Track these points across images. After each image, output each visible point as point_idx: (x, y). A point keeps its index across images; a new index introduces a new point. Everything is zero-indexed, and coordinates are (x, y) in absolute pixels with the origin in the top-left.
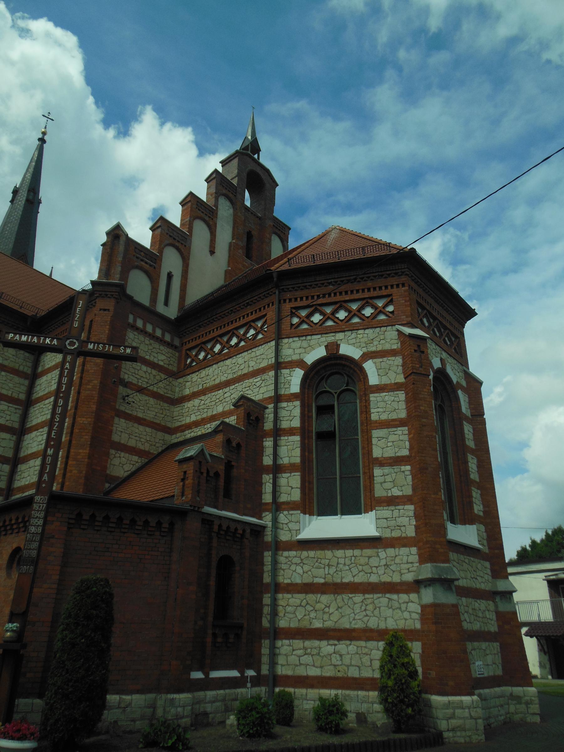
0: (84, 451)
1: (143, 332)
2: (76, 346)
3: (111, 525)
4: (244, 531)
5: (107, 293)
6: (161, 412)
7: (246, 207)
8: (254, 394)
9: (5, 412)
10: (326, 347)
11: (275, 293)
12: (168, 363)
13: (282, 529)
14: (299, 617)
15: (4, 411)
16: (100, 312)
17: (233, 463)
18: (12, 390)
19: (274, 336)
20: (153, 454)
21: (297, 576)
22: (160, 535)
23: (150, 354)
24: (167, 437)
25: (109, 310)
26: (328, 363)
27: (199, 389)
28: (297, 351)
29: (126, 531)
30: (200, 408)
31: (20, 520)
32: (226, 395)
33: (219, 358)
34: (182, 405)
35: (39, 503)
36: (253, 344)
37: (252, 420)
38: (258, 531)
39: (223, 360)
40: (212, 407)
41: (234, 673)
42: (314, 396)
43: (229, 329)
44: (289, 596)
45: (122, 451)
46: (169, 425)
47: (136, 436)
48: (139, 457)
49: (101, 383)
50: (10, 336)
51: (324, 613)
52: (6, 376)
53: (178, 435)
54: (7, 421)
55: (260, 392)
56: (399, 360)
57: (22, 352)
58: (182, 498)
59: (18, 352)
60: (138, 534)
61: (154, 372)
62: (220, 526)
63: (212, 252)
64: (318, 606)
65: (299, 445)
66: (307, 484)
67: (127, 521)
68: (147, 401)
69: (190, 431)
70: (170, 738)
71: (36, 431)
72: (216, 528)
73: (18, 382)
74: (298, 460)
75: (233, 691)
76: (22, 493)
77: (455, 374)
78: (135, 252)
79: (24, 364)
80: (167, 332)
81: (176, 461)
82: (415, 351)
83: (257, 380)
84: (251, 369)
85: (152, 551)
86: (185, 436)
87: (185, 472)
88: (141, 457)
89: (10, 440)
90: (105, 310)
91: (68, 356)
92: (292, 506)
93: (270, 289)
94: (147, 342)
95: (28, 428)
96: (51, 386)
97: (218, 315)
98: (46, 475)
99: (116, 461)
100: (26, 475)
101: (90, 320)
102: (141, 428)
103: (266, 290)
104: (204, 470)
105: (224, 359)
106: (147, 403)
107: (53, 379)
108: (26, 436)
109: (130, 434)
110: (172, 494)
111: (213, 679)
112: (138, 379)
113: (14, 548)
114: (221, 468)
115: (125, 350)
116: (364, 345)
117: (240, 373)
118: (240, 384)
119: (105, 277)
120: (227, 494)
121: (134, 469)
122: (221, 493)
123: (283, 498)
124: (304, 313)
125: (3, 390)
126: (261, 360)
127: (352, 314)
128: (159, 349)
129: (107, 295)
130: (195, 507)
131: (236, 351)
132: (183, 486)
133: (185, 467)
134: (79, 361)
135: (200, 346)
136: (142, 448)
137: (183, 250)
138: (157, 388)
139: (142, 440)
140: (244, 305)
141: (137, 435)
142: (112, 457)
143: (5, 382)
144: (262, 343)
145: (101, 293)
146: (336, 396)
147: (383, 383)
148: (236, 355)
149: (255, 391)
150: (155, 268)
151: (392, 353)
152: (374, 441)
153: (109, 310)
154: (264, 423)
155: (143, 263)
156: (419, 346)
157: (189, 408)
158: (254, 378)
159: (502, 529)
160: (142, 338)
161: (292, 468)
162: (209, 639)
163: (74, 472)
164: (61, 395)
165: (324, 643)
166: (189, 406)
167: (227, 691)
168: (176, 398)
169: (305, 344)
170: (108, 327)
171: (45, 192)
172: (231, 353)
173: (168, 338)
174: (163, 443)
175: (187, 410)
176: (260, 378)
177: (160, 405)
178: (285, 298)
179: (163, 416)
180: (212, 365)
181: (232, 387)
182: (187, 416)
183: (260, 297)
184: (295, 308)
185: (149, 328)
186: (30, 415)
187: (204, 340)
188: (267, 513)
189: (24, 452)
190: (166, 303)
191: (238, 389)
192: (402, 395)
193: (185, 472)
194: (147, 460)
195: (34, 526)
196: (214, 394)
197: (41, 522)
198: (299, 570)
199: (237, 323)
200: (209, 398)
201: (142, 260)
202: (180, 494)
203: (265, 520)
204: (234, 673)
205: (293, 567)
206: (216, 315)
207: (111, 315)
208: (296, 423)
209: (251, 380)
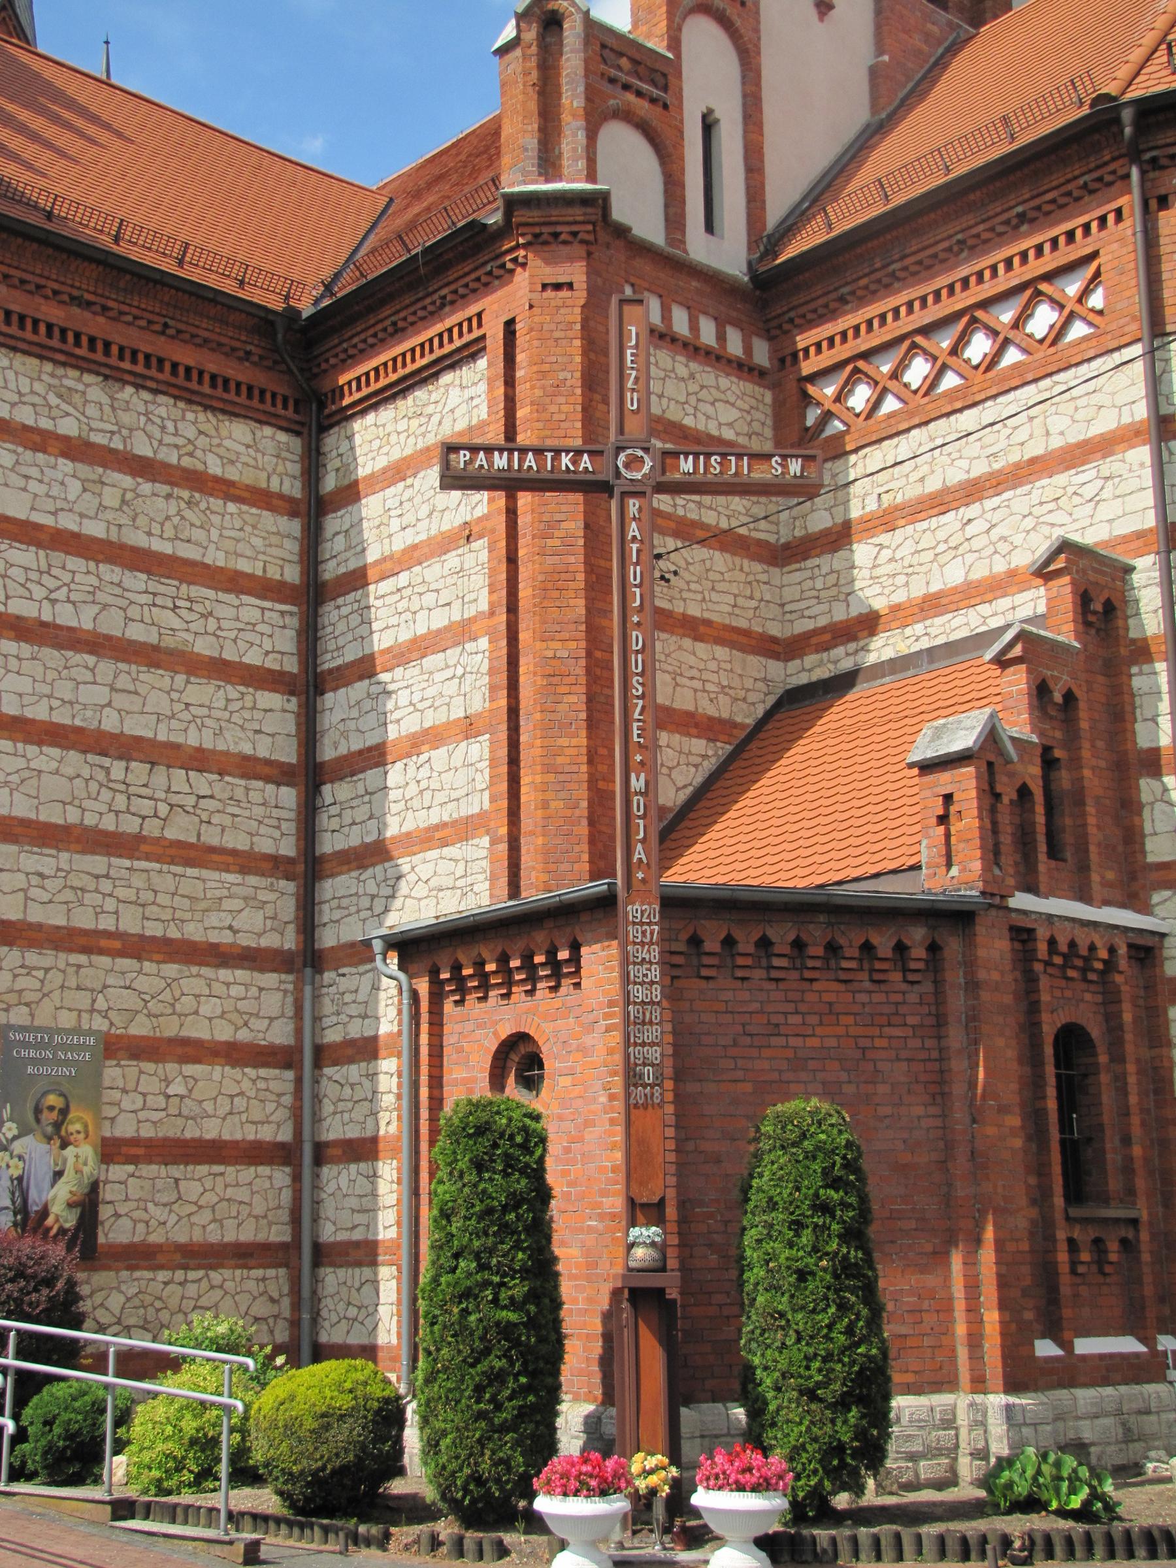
0: (574, 741)
2: (646, 469)
3: (776, 962)
4: (1112, 950)
5: (559, 229)
6: (748, 593)
8: (1077, 526)
9: (258, 628)
11: (1127, 176)
12: (746, 429)
15: (254, 625)
16: (545, 294)
17: (1058, 753)
18: (261, 557)
19: (1134, 327)
20: (743, 726)
22: (905, 981)
23: (695, 408)
24: (775, 668)
25: (570, 286)
27: (868, 509)
29: (815, 975)
30: (878, 572)
32: (970, 530)
34: (809, 563)
35: (642, 923)
37: (1095, 613)
39: (948, 415)
40: (923, 569)
41: (1129, 1345)
43: (959, 306)
46: (774, 630)
47: (692, 678)
48: (709, 740)
49: (587, 526)
50: (462, 460)
52: (241, 513)
53: (810, 660)
54: (267, 653)
55: (1096, 520)
57: (268, 431)
58: (948, 870)
59: (259, 434)
60: (845, 982)
62: (1052, 942)
67: (816, 950)
68: (708, 563)
70: (1073, 1491)
71: (367, 682)
72: (1042, 948)
73: (274, 529)
75: (1136, 1389)
76: (358, 868)
78: (605, 61)
79: (280, 469)
80: (730, 323)
81: (911, 766)
85: (889, 1025)
86: (836, 662)
88: (714, 740)
89: (285, 711)
90: (558, 287)
91: (631, 501)
93: (1106, 164)
94: (682, 371)
95: (331, 671)
96: (390, 536)
97: (907, 262)
98: (639, 847)
100: (361, 814)
101: (505, 318)
102: (701, 648)
103: (1092, 165)
104: (1009, 794)
105: (949, 409)
106: (708, 570)
107: (393, 513)
108: (329, 696)
109: (674, 673)
110: (912, 861)
111: (1084, 1358)
113: (503, 1036)
115: (784, 466)
117: (1015, 457)
118: (1019, 491)
119: (540, 174)
121: (699, 780)
122: (1042, 847)
125: (240, 560)
126: (1092, 411)
128: (718, 388)
129: (556, 235)
130: (993, 895)
132: (948, 835)
133: (945, 781)
135: (849, 368)
136: (712, 711)
137: (738, 23)
138: (729, 517)
139: (710, 687)
140: (1007, 222)
141: (695, 673)
143: (241, 534)
144: (1091, 354)
145: (537, 230)
148: (995, 397)
149: (1079, 513)
153: (570, 286)
154: (1126, 618)
155: (630, 97)
157: (838, 572)
158: (1073, 472)
162: (1063, 1257)
163: (553, 805)
164: (635, 619)
166: (836, 566)
167: (1123, 1389)
168: (782, 541)
170: (577, 343)
172: (975, 389)
173: (735, 345)
174: (765, 689)
175: (832, 579)
176: (1093, 473)
177: (741, 570)
178: (1163, 191)
179: (754, 604)
180: (908, 430)
181: (989, 503)
182: (835, 599)
183: (1069, 194)
186: (329, 629)
187: (865, 343)
188: (1167, 893)
189: (336, 746)
190: (710, 227)
191: (1014, 510)
193: (948, 798)
194: (729, 748)
195: (642, 984)
196: (925, 525)
199: (986, 286)
200: (909, 542)
201: (626, 87)
202: (943, 860)
203: (1162, 915)
204: (1129, 1345)
206: (902, 259)
207: (582, 302)
209: (1061, 479)
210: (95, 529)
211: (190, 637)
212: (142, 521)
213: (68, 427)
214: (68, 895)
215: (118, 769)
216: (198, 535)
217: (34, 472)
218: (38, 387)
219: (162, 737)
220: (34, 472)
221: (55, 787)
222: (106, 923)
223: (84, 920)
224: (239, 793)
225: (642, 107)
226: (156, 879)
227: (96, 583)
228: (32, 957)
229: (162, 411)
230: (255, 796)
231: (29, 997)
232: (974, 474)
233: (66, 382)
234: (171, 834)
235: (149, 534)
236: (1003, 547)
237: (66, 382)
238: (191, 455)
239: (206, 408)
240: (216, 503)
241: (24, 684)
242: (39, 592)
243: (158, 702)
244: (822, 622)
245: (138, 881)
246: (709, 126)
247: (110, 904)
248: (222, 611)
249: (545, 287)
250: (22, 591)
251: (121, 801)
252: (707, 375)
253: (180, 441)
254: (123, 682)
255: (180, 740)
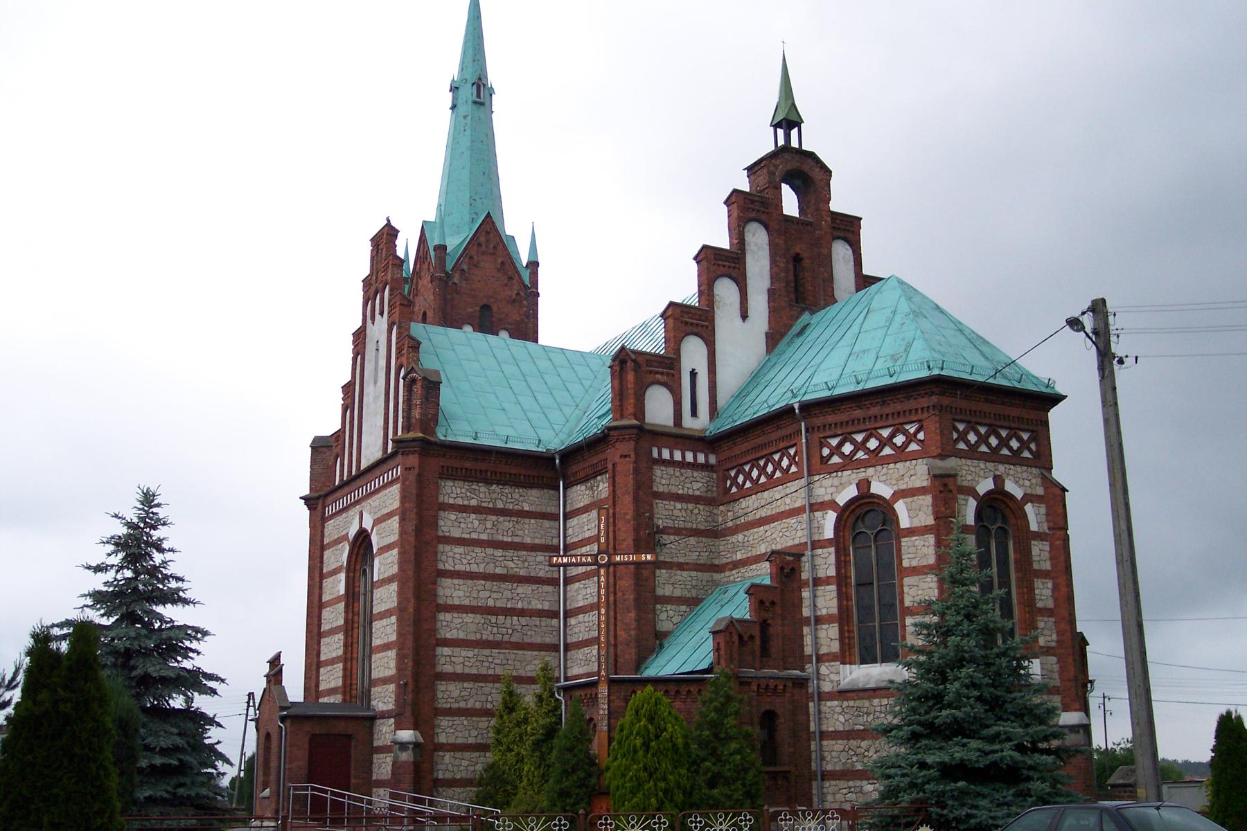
1: (671, 463)
7: (789, 219)
10: (857, 485)
12: (704, 489)
13: (824, 680)
14: (844, 761)
21: (840, 724)
25: (629, 456)
26: (862, 501)
28: (830, 490)
31: (588, 697)
33: (758, 489)
36: (787, 478)
38: (801, 683)
42: (851, 538)
44: (834, 742)
45: (667, 604)
46: (716, 562)
51: (865, 756)
56: (928, 499)
57: (546, 491)
61: (690, 506)
63: (744, 316)
64: (859, 751)
65: (835, 595)
66: (846, 635)
69: (737, 570)
74: (834, 611)
77: (1020, 486)
82: (941, 492)
83: (792, 521)
84: (787, 508)
87: (718, 643)
92: (832, 657)
99: (663, 616)
100: (577, 630)
102: (685, 574)
104: (735, 638)
112: (673, 520)
114: (756, 632)
116: (894, 482)
120: (765, 651)
123: (823, 650)
124: (834, 442)
127: (883, 443)
129: (624, 438)
131: (772, 483)
132: (719, 655)
134: (611, 569)
136: (688, 595)
139: (688, 587)
142: (658, 612)
146: (872, 537)
147: (914, 526)
150: (673, 375)
151: (921, 491)
152: (906, 589)
153: (629, 456)
156: (945, 485)
159: (1122, 654)
160: (671, 470)
161: (829, 619)
165: (865, 782)
169: (836, 482)
170: (631, 476)
171: (494, 77)
173: (701, 458)
179: (707, 554)
182: (733, 552)
184: (823, 438)
185: (678, 456)
192: (931, 539)
193: (718, 643)
197: (606, 707)
198: (841, 719)
201: (657, 373)
205: (836, 716)
208: (832, 572)
210: (484, 537)
211: (517, 570)
212: (500, 531)
213: (474, 502)
214: (477, 664)
215: (493, 619)
216: (520, 533)
217: (462, 520)
218: (464, 491)
219: (509, 606)
220: (462, 520)
221: (472, 627)
222: (491, 672)
223: (484, 671)
224: (538, 623)
225: (664, 379)
226: (508, 656)
227: (484, 555)
228: (466, 685)
229: (506, 491)
230: (543, 624)
231: (466, 698)
232: (768, 514)
233: (473, 487)
234: (513, 640)
235: (503, 535)
236: (775, 542)
237: (473, 487)
238: (517, 504)
239: (523, 487)
240: (527, 520)
241: (461, 594)
242: (465, 561)
243: (508, 594)
244: (730, 560)
245: (501, 656)
246: (693, 374)
247: (492, 666)
248: (530, 559)
249: (621, 456)
250: (459, 562)
251: (495, 630)
252: (689, 473)
253: (513, 500)
254: (495, 588)
255: (515, 606)
